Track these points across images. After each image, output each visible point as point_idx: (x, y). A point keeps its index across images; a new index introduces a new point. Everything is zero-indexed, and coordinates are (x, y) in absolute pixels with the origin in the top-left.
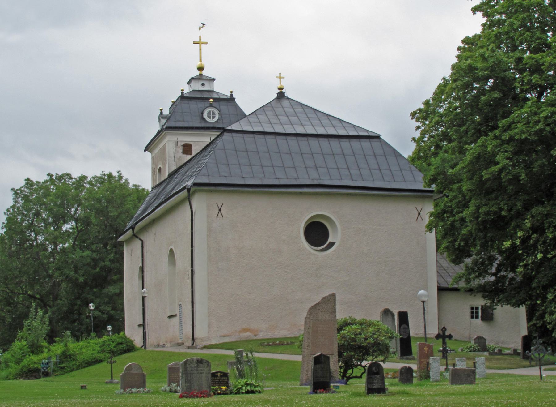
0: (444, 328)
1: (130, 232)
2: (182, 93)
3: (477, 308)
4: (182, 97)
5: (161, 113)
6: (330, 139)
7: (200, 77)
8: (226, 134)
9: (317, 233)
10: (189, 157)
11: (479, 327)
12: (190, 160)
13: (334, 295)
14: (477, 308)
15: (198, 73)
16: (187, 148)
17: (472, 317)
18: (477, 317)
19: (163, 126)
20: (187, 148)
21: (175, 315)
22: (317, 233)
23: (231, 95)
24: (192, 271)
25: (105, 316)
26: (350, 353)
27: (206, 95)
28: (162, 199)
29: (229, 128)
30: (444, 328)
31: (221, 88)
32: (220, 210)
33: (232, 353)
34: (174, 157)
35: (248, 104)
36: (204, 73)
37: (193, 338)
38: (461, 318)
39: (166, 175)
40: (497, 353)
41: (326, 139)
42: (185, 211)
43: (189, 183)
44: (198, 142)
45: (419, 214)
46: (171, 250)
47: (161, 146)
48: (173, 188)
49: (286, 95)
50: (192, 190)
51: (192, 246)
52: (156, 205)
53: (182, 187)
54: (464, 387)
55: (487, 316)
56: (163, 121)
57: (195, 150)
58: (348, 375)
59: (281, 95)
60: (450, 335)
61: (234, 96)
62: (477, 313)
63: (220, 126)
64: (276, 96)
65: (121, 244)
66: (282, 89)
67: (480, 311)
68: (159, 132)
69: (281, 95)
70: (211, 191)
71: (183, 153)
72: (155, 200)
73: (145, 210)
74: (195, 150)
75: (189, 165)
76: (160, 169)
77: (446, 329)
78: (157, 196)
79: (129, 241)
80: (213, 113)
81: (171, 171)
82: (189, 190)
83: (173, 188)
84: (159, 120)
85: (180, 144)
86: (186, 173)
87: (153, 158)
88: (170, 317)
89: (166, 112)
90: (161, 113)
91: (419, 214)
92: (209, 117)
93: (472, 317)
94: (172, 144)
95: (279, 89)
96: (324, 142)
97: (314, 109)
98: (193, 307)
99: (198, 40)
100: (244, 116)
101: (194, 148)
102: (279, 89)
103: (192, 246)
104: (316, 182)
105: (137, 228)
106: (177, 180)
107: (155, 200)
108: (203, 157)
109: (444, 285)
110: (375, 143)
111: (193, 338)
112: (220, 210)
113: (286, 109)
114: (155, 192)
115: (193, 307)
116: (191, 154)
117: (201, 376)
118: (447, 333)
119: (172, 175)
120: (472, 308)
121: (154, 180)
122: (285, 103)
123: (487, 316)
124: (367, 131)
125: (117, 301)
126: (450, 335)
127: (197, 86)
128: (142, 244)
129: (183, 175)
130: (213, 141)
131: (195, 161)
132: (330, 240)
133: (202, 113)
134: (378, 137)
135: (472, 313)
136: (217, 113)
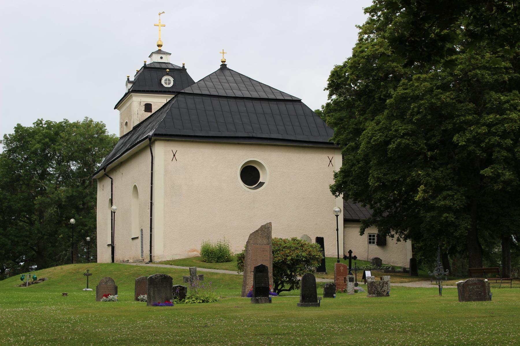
0: (350, 250)
1: (102, 172)
2: (145, 64)
3: (374, 236)
4: (145, 67)
5: (128, 79)
6: (262, 102)
7: (159, 52)
8: (180, 95)
9: (250, 175)
10: (149, 114)
11: (375, 251)
12: (151, 116)
13: (270, 223)
14: (374, 236)
15: (157, 48)
16: (148, 107)
17: (370, 243)
18: (373, 243)
19: (129, 89)
20: (148, 107)
21: (137, 238)
22: (250, 175)
23: (184, 66)
24: (151, 203)
25: (405, 137)
26: (283, 269)
27: (164, 66)
28: (128, 146)
29: (183, 91)
30: (350, 250)
31: (175, 60)
32: (174, 155)
33: (188, 268)
34: (138, 115)
35: (197, 74)
36: (162, 49)
37: (151, 256)
38: (360, 244)
39: (132, 129)
40: (392, 271)
41: (259, 102)
42: (146, 158)
43: (151, 134)
44: (158, 102)
45: (331, 161)
46: (135, 187)
47: (128, 105)
48: (137, 138)
49: (227, 66)
50: (152, 140)
51: (152, 184)
52: (124, 150)
53: (144, 137)
54: (474, 305)
55: (382, 242)
56: (130, 86)
57: (154, 109)
58: (279, 288)
59: (224, 67)
60: (355, 256)
61: (185, 67)
62: (374, 239)
63: (174, 90)
64: (219, 67)
65: (95, 181)
66: (225, 62)
67: (376, 238)
68: (126, 95)
69: (224, 67)
70: (168, 140)
71: (145, 111)
72: (123, 147)
73: (114, 155)
74: (154, 109)
75: (150, 120)
76: (127, 123)
77: (352, 252)
78: (125, 144)
79: (101, 179)
80: (169, 80)
81: (135, 125)
82: (150, 139)
83: (137, 138)
84: (127, 85)
85: (143, 104)
86: (147, 126)
87: (121, 114)
88: (133, 239)
89: (132, 79)
90: (128, 79)
91: (331, 161)
92: (166, 83)
93: (370, 243)
94: (138, 101)
95: (222, 62)
96: (257, 104)
97: (250, 78)
98: (151, 231)
99: (157, 23)
100: (194, 83)
101: (153, 107)
102: (222, 62)
103: (152, 184)
104: (251, 135)
105: (108, 169)
106: (140, 132)
107: (123, 147)
108: (161, 113)
109: (349, 217)
110: (297, 105)
111: (151, 256)
112: (174, 155)
113: (227, 78)
114: (122, 141)
115: (151, 231)
116: (151, 112)
117: (161, 287)
118: (353, 255)
119: (136, 128)
120: (370, 236)
121: (121, 132)
122: (227, 73)
123: (382, 242)
124: (291, 96)
125: (90, 228)
126: (355, 256)
127: (157, 58)
128: (112, 181)
129: (145, 128)
130: (169, 101)
131: (155, 116)
132: (261, 180)
133: (161, 80)
134: (299, 101)
135: (370, 239)
136: (172, 79)
